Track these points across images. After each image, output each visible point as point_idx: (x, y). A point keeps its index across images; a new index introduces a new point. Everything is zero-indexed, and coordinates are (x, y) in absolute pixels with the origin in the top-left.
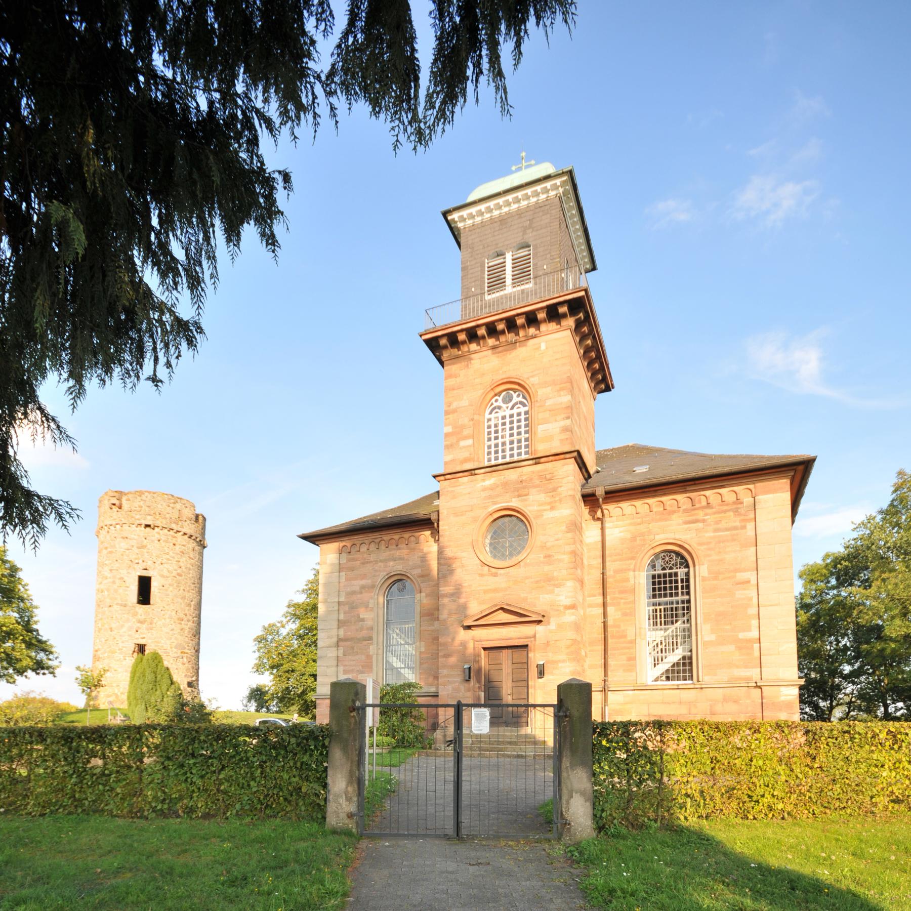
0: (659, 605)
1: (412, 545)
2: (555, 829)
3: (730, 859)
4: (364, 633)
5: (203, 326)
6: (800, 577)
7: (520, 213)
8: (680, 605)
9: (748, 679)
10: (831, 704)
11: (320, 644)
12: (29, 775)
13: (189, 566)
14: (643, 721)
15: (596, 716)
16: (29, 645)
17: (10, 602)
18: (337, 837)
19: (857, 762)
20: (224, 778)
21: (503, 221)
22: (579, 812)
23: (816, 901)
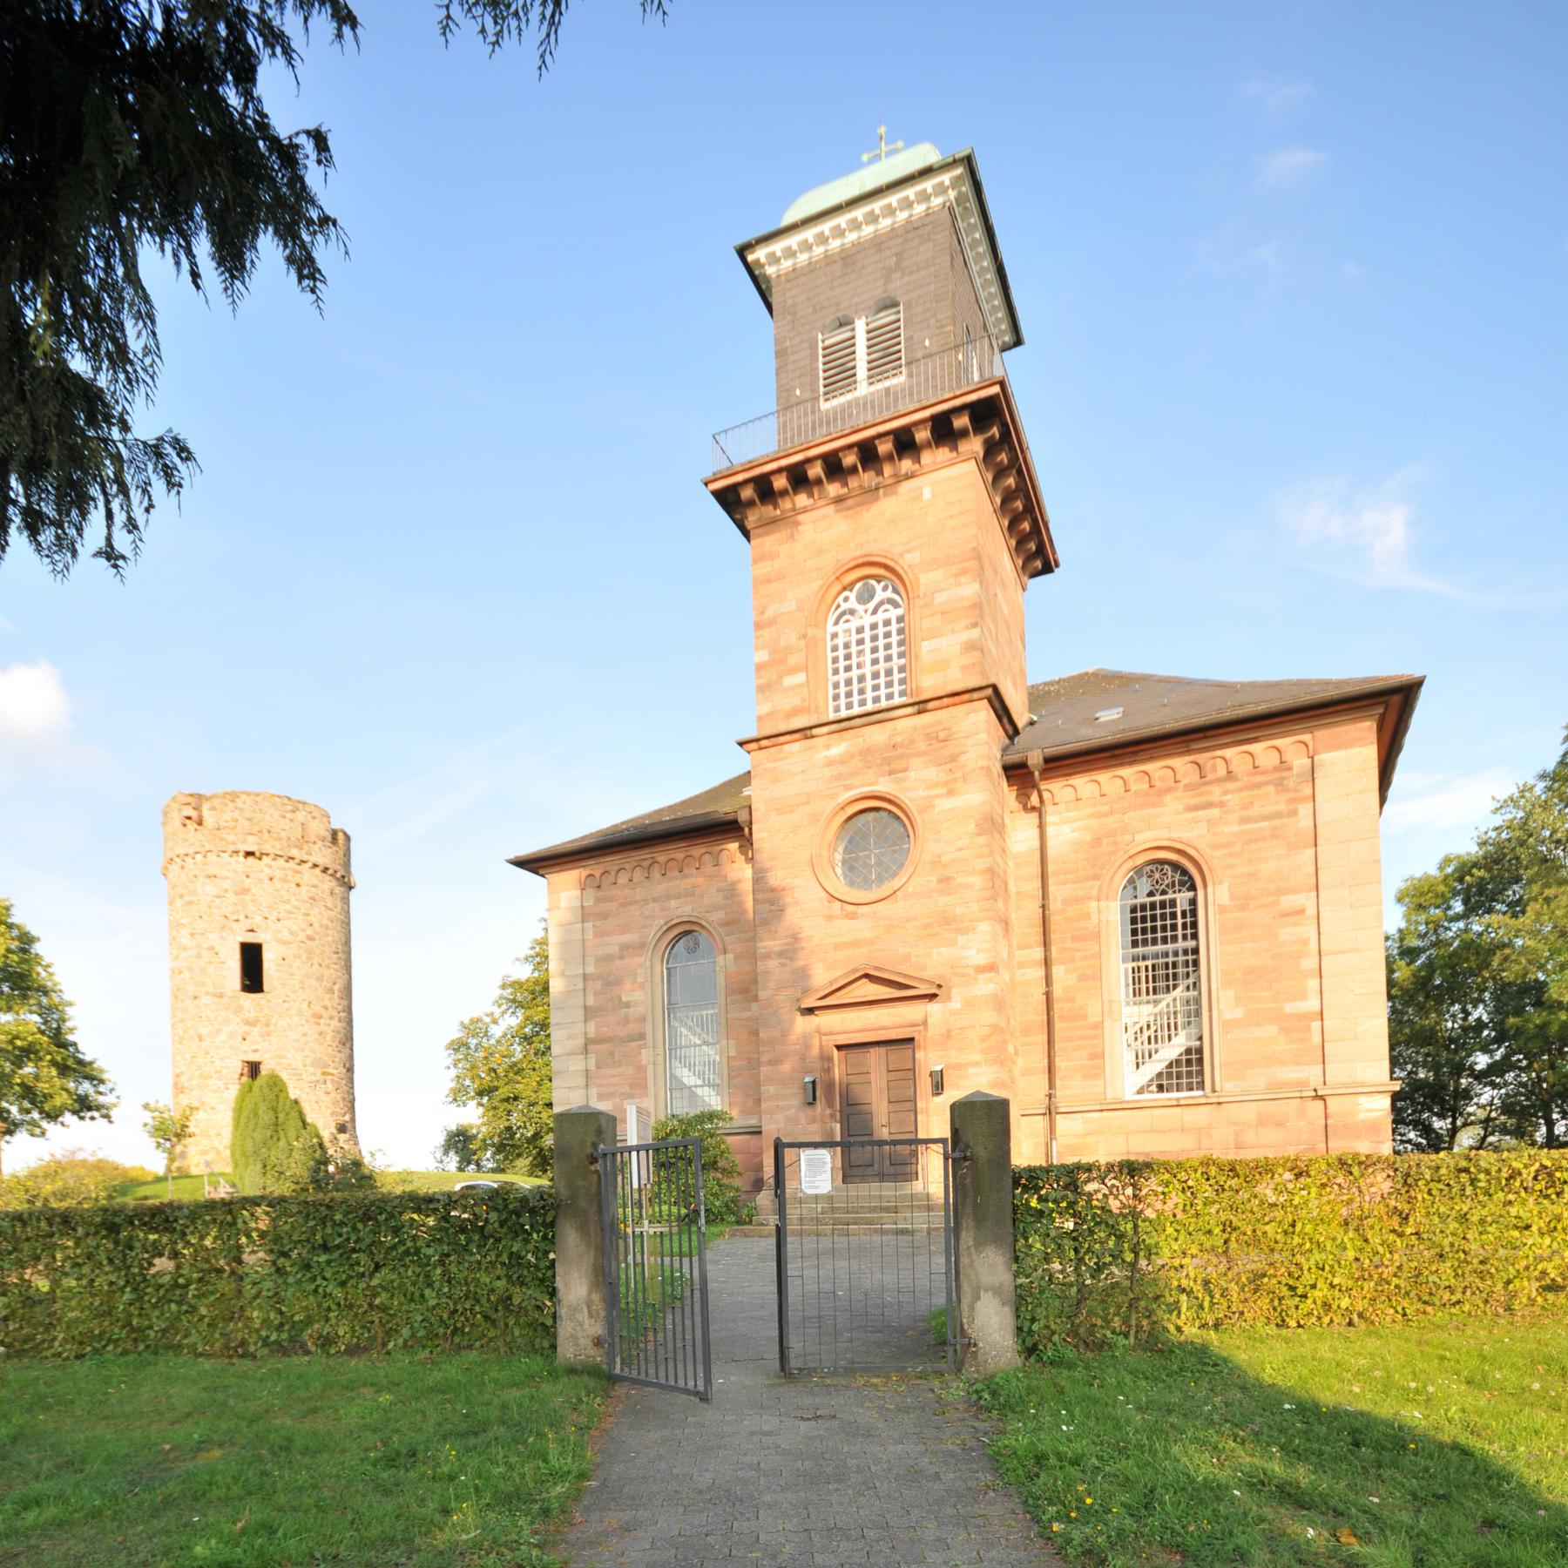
0: (1144, 958)
2: (950, 1354)
3: (1251, 1397)
4: (633, 1027)
6: (1399, 900)
7: (878, 243)
8: (1181, 958)
9: (1301, 1085)
10: (1453, 1123)
11: (555, 1050)
12: (52, 1291)
13: (325, 921)
14: (1103, 1162)
15: (1025, 1152)
16: (64, 1070)
17: (25, 997)
18: (574, 1379)
19: (1482, 1221)
20: (380, 1285)
21: (847, 258)
22: (992, 1325)
23: (1394, 1464)
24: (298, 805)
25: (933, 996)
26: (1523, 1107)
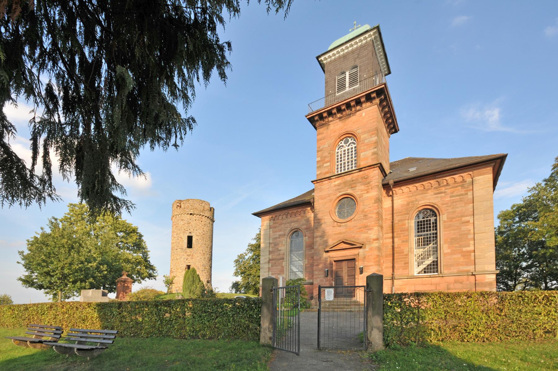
0: (421, 236)
1: (302, 214)
2: (364, 345)
4: (281, 256)
5: (196, 119)
6: (498, 218)
7: (353, 52)
8: (432, 236)
9: (468, 271)
10: (515, 283)
11: (261, 262)
15: (386, 290)
16: (146, 267)
17: (139, 250)
18: (264, 348)
19: (526, 312)
21: (345, 57)
22: (376, 337)
24: (203, 202)
25: (361, 247)
26: (538, 278)
